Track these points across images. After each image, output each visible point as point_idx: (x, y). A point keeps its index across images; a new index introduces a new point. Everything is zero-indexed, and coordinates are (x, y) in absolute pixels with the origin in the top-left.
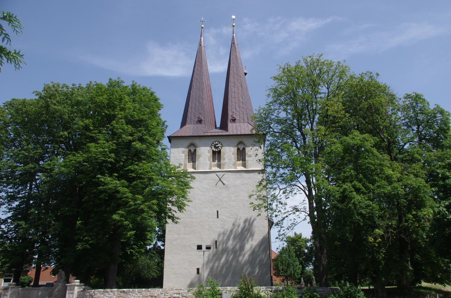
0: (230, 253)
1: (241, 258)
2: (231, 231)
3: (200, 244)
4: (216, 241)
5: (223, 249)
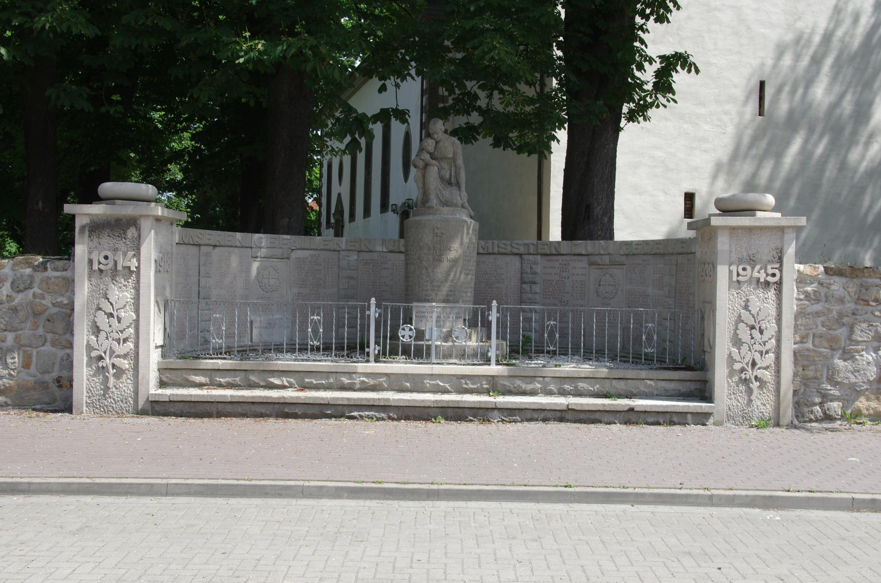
0: (819, 129)
1: (854, 155)
2: (827, 38)
3: (690, 190)
4: (762, 84)
5: (791, 112)
